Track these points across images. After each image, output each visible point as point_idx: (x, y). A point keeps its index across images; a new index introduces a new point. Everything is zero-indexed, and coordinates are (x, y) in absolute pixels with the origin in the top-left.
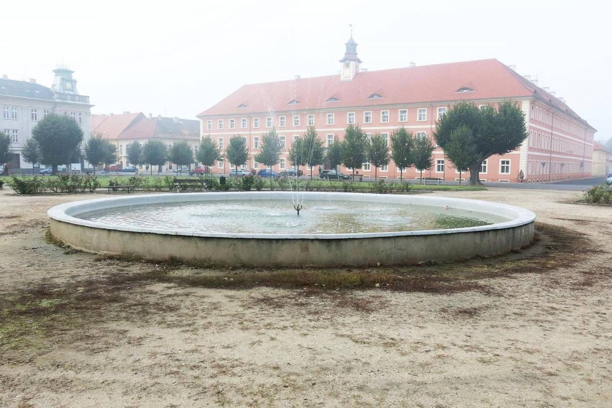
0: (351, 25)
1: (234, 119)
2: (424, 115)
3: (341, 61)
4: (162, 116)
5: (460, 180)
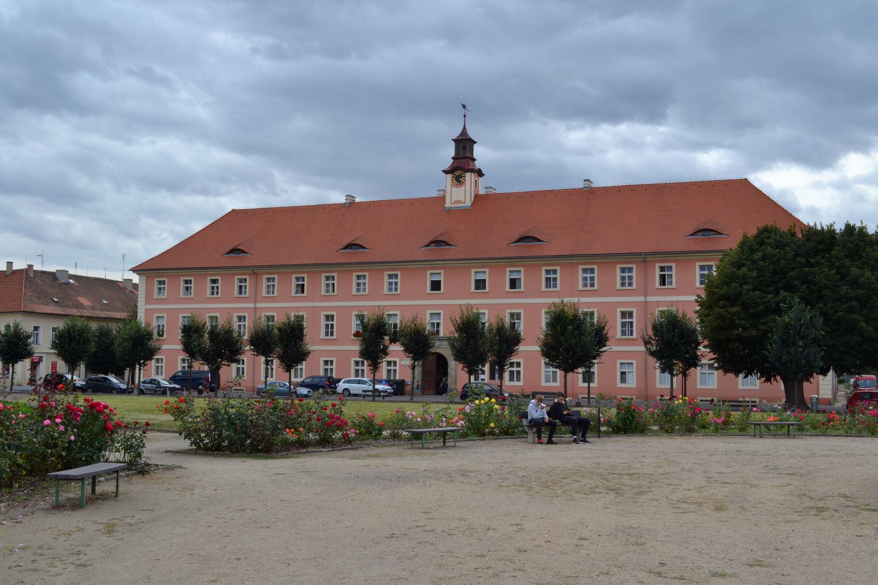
0: (464, 107)
2: (364, 284)
3: (446, 172)
4: (35, 268)
5: (589, 398)
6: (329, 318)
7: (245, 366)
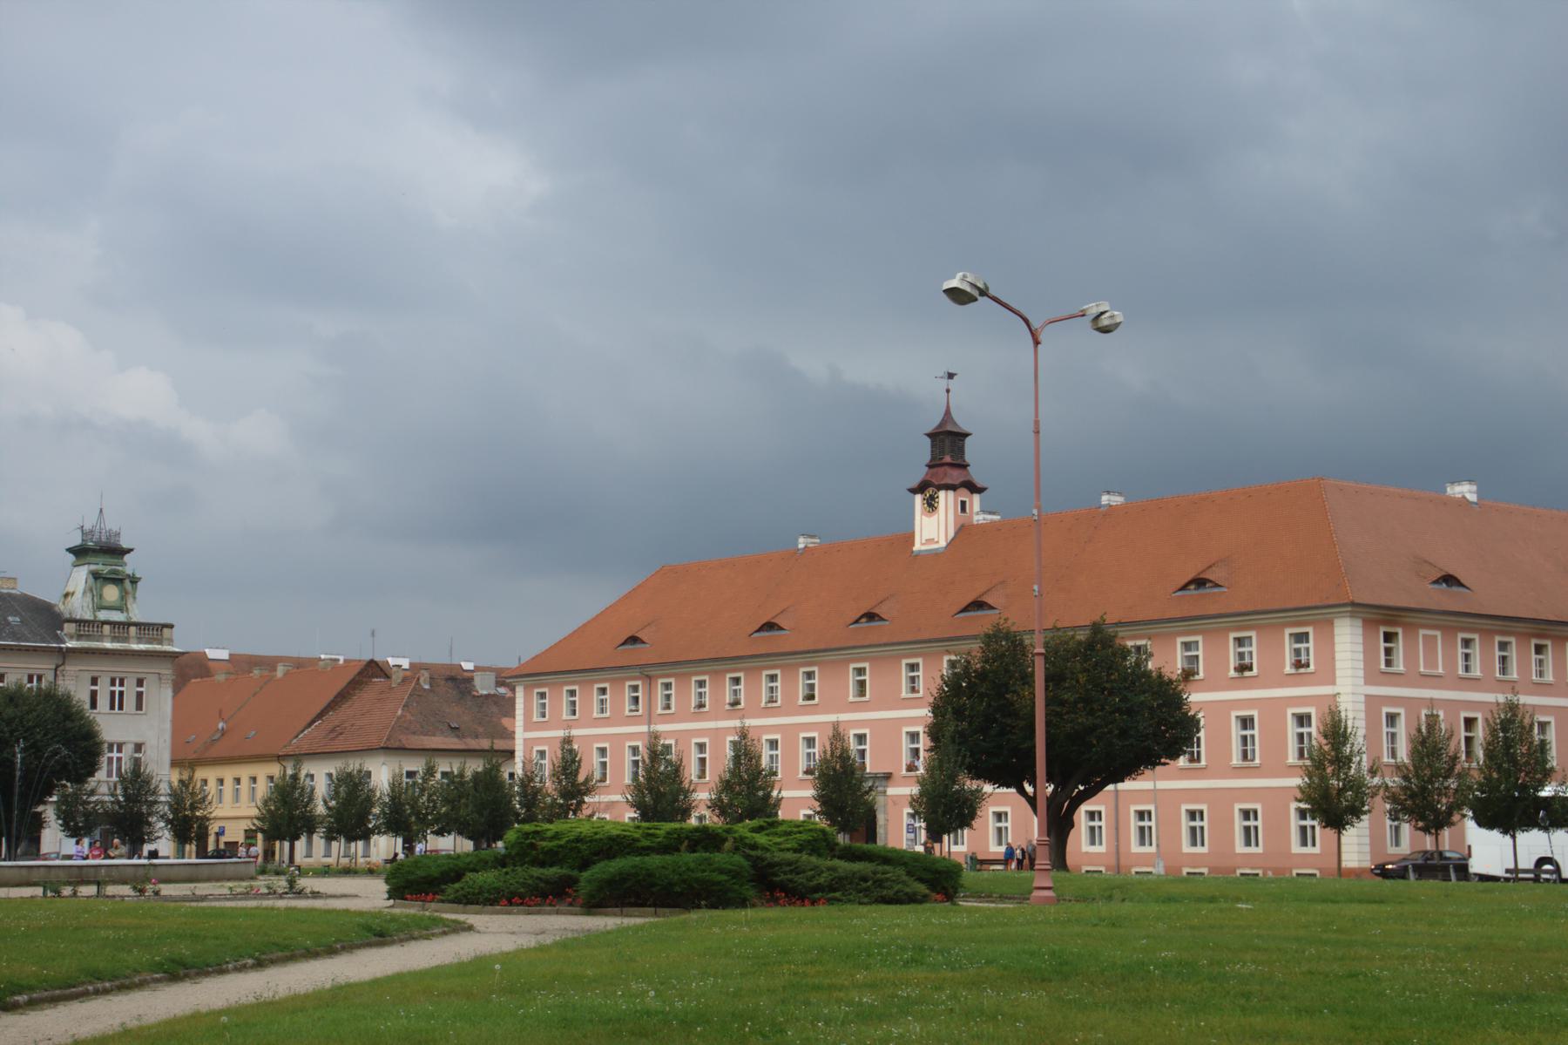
1: (606, 685)
6: (1246, 722)
7: (1259, 823)
